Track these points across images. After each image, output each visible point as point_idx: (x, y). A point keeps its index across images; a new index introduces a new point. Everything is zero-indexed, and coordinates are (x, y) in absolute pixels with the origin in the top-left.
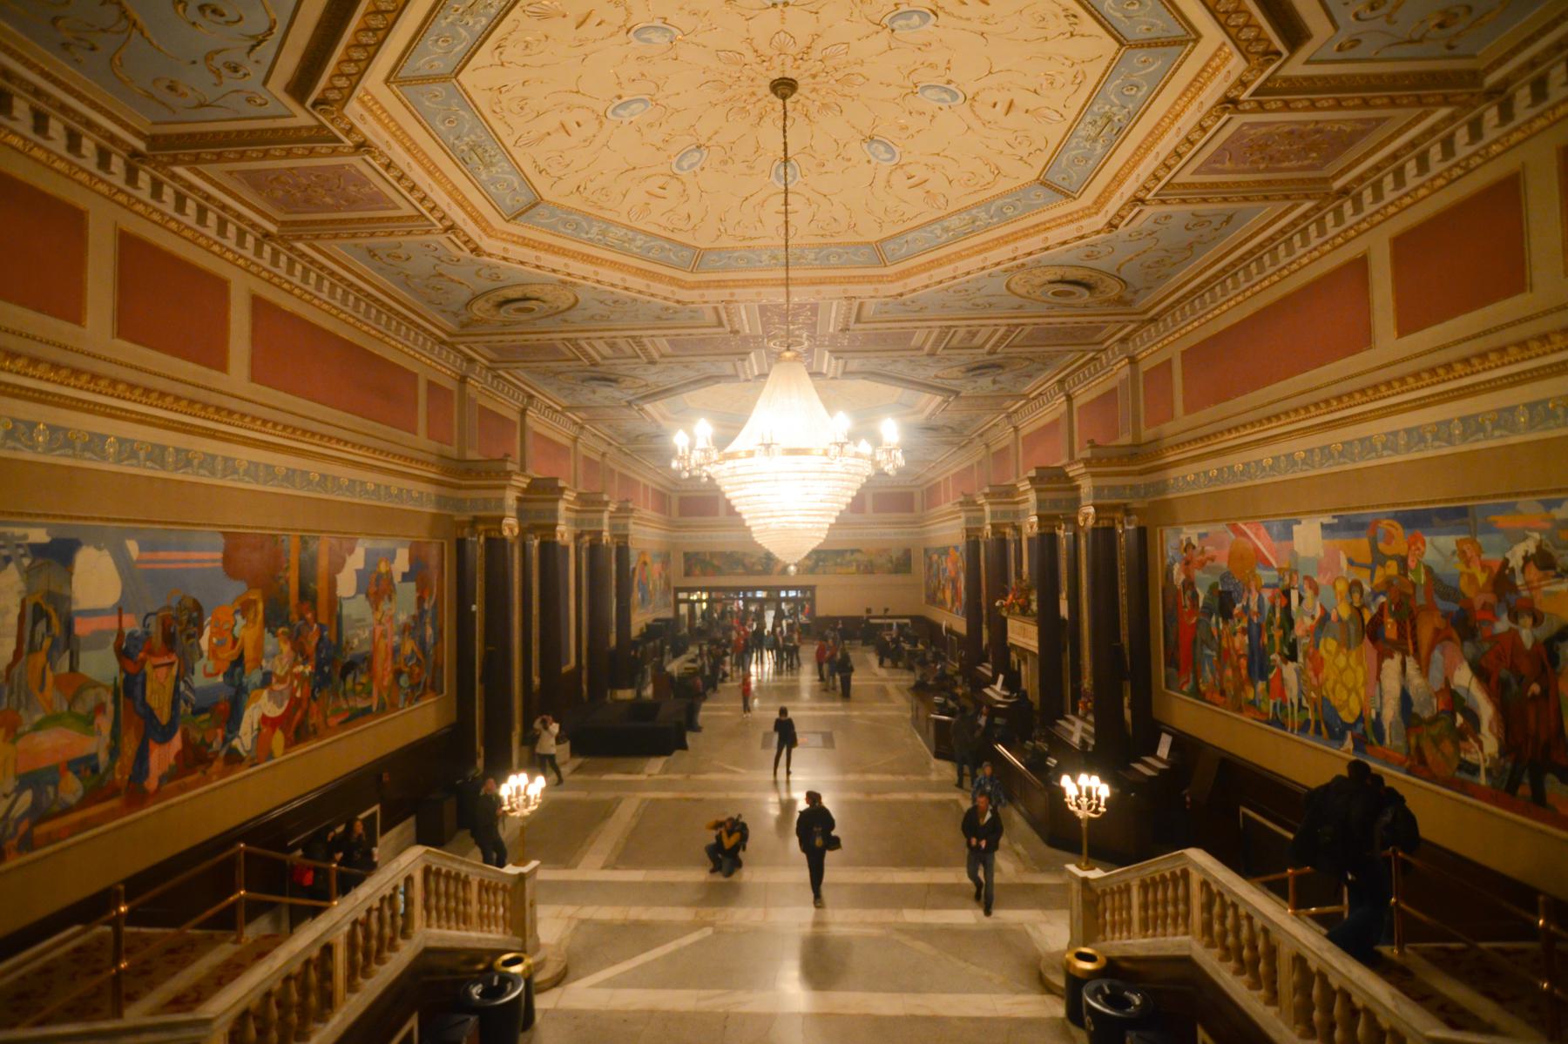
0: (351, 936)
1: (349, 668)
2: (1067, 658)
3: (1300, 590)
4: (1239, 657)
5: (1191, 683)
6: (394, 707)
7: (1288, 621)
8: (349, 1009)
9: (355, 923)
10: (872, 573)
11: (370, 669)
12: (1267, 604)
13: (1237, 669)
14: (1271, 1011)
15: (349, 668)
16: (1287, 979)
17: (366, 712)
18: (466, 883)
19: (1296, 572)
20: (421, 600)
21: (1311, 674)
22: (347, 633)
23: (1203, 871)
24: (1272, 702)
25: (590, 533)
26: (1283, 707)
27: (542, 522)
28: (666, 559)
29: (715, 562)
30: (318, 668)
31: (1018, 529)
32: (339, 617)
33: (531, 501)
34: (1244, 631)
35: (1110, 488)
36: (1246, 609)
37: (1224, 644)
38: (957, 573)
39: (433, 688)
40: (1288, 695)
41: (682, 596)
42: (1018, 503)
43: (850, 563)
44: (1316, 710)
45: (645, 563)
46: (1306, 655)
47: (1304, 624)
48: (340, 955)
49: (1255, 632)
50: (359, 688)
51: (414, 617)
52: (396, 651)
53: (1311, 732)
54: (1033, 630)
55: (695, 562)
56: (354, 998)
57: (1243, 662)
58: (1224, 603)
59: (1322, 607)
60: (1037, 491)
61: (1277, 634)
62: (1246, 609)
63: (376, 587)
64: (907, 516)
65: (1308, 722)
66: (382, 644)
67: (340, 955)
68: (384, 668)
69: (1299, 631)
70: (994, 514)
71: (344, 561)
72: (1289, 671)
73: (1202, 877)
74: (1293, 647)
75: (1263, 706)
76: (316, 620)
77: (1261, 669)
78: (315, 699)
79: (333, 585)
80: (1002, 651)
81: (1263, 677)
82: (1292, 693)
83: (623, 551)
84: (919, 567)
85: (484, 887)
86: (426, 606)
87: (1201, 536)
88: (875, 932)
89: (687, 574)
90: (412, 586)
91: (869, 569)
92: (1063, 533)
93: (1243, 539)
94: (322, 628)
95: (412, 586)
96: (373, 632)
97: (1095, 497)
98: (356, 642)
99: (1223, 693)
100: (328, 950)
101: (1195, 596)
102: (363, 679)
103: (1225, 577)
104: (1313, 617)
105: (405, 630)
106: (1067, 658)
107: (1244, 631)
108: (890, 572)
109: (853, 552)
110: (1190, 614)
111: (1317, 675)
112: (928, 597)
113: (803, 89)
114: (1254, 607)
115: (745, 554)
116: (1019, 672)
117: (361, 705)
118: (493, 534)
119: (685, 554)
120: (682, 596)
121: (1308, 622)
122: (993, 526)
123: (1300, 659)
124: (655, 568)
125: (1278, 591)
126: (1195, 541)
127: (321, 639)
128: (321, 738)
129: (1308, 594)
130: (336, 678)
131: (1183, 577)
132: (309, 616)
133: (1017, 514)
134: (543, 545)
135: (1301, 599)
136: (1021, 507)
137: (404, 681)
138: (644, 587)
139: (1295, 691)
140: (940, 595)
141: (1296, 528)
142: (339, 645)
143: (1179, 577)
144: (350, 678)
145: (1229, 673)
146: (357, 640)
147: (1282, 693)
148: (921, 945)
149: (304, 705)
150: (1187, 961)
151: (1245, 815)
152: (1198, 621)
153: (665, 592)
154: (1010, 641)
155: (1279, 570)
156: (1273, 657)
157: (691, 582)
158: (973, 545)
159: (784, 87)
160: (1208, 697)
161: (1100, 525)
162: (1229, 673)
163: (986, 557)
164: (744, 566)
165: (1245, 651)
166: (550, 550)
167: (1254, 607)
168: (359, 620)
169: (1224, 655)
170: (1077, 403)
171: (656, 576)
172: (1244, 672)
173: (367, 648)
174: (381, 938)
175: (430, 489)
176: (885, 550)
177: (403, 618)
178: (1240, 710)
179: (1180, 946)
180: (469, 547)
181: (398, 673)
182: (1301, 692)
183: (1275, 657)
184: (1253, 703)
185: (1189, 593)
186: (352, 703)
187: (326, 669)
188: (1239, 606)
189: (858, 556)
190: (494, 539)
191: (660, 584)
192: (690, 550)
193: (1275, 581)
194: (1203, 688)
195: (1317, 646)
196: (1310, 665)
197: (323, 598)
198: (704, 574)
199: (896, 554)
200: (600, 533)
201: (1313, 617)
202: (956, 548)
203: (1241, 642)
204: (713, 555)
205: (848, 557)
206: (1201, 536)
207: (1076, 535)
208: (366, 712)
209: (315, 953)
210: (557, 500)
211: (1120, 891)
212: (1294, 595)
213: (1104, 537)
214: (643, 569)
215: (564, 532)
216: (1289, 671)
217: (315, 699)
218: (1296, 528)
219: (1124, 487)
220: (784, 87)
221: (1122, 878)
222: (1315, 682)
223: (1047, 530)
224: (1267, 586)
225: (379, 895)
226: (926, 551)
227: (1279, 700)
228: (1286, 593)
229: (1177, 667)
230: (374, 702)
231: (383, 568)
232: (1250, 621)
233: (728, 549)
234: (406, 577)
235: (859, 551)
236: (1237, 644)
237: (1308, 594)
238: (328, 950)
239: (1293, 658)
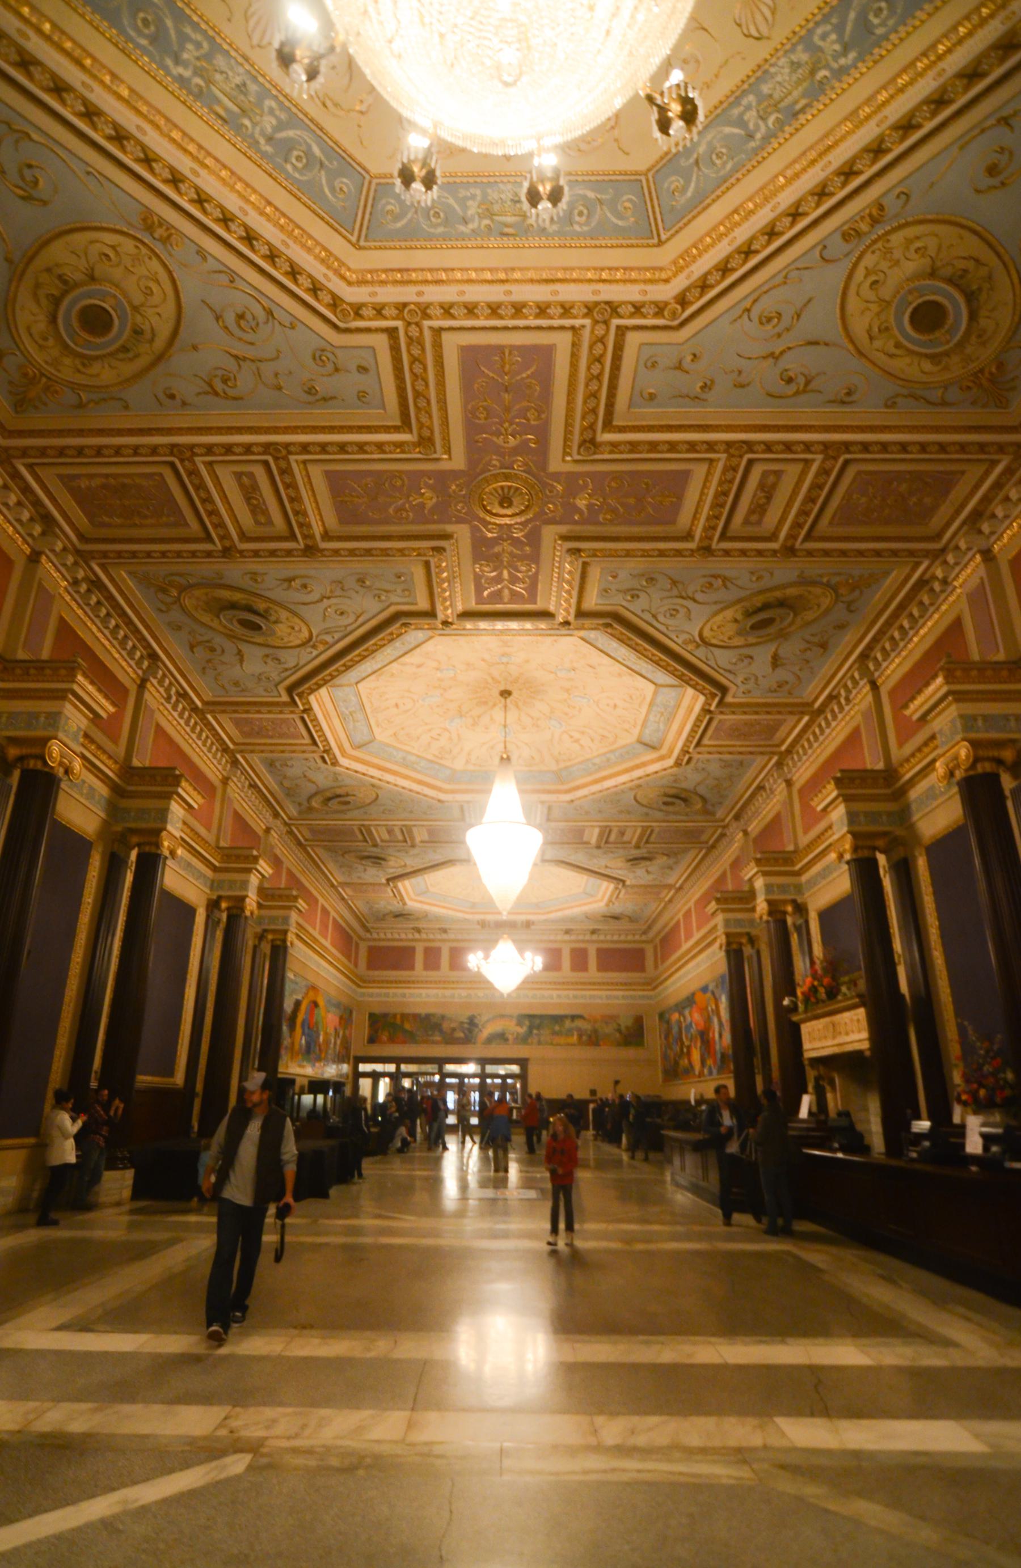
25: (229, 898)
27: (143, 825)
28: (346, 1017)
29: (407, 1026)
31: (801, 909)
33: (132, 795)
35: (986, 718)
42: (798, 874)
43: (569, 1033)
45: (315, 1004)
55: (387, 1028)
60: (848, 799)
64: (635, 976)
70: (769, 888)
84: (654, 1038)
88: (722, 1472)
89: (372, 1040)
91: (593, 1039)
97: (966, 728)
108: (619, 1045)
109: (573, 1018)
113: (515, 694)
115: (443, 1017)
118: (31, 764)
119: (371, 1015)
122: (770, 902)
133: (799, 888)
140: (684, 1062)
148: (871, 1512)
157: (375, 1050)
159: (506, 694)
161: (980, 769)
164: (441, 1031)
170: (884, 691)
171: (331, 1030)
176: (613, 1018)
189: (579, 1023)
190: (35, 773)
192: (377, 1010)
198: (392, 1040)
199: (626, 1022)
200: (243, 899)
204: (404, 1016)
205: (568, 1024)
210: (168, 796)
215: (183, 879)
219: (1006, 717)
220: (506, 694)
223: (866, 853)
226: (661, 1016)
233: (423, 1011)
235: (581, 1017)
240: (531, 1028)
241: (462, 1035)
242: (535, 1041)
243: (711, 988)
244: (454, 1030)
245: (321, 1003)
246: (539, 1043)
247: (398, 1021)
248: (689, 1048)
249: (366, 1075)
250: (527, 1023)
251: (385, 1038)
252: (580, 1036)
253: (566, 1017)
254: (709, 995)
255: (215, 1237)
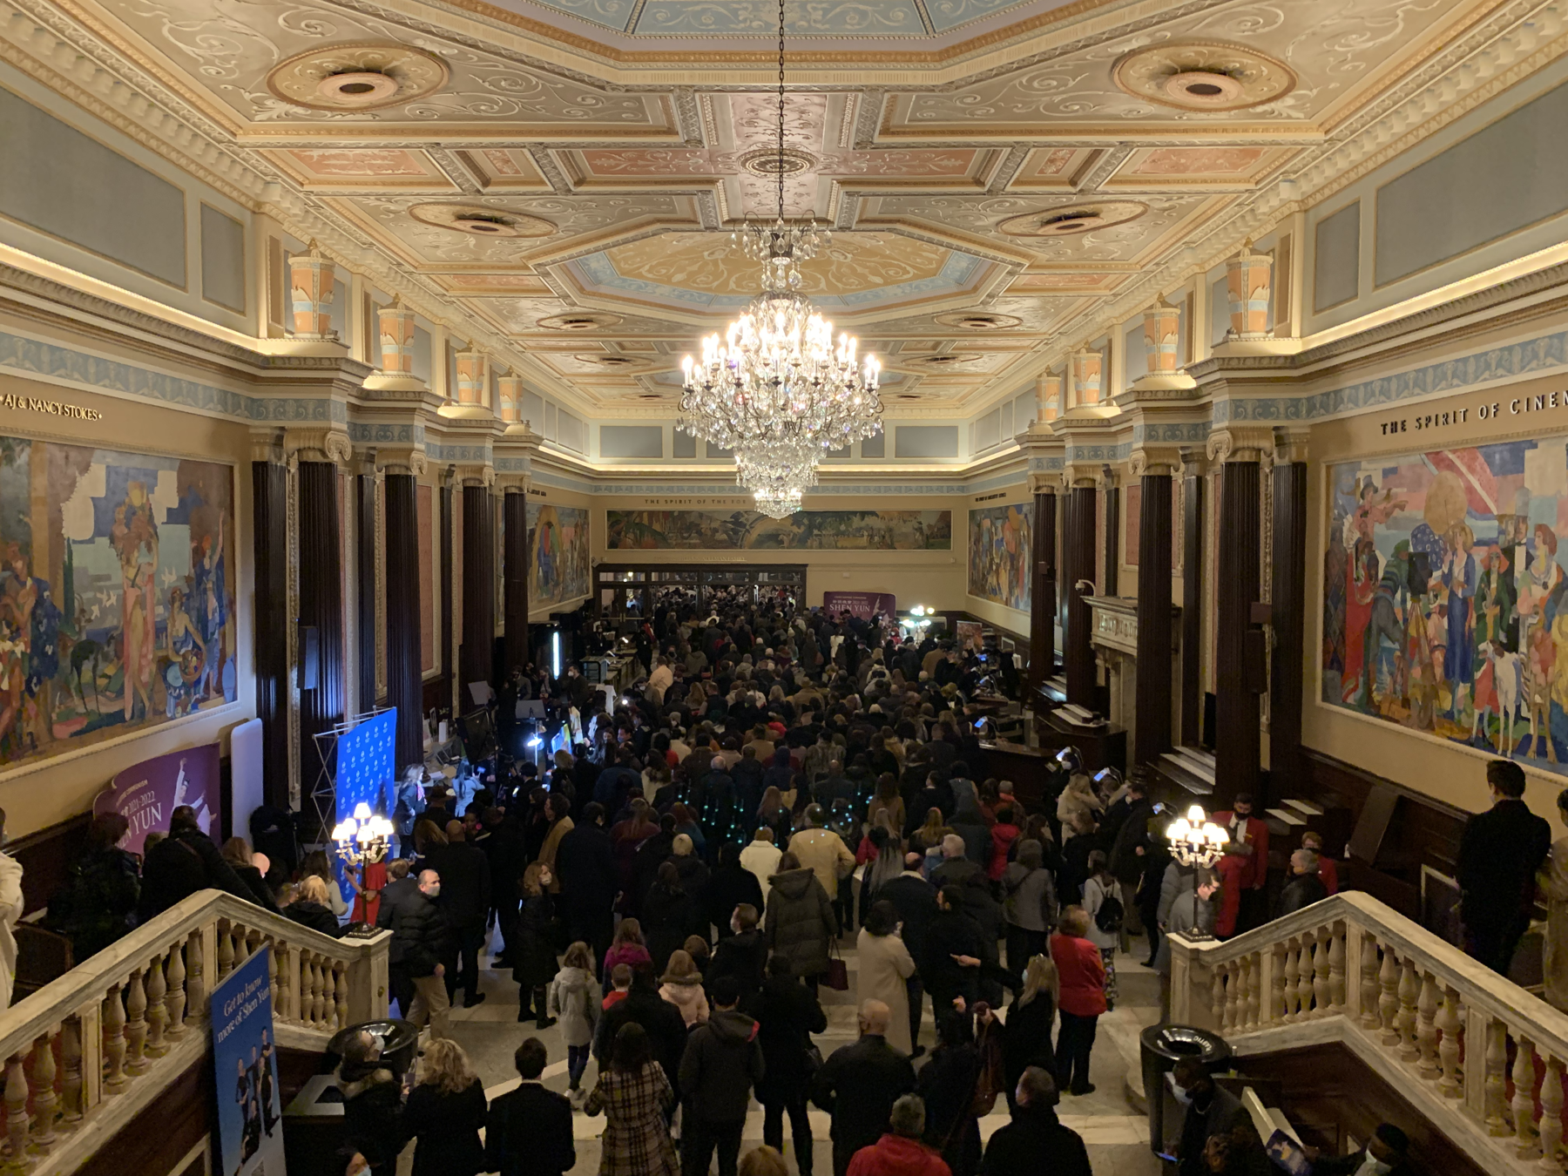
0: (107, 1005)
1: (86, 650)
2: (1178, 665)
3: (1530, 545)
4: (1433, 649)
5: (1360, 691)
6: (160, 715)
7: (1509, 593)
8: (110, 1113)
9: (113, 990)
10: (891, 547)
11: (119, 654)
12: (1479, 570)
13: (1428, 667)
14: (1453, 1104)
15: (86, 650)
16: (1482, 1051)
17: (116, 719)
18: (281, 951)
19: (1525, 519)
20: (198, 554)
21: (1537, 668)
22: (83, 596)
23: (1368, 919)
24: (1477, 713)
25: (463, 468)
26: (1493, 720)
29: (657, 527)
30: (36, 646)
32: (68, 571)
34: (1443, 611)
36: (1447, 578)
37: (1412, 632)
38: (1019, 545)
39: (220, 691)
40: (1501, 701)
41: (606, 577)
44: (1541, 721)
45: (549, 525)
46: (1531, 640)
47: (1531, 595)
48: (92, 1033)
49: (1455, 611)
50: (102, 682)
51: (188, 579)
52: (160, 630)
53: (1531, 753)
54: (1131, 623)
56: (114, 1102)
57: (1439, 656)
58: (1415, 570)
59: (1559, 568)
61: (1491, 612)
62: (1447, 578)
63: (125, 527)
65: (1528, 737)
66: (138, 617)
67: (92, 1033)
68: (140, 652)
69: (1522, 608)
71: (72, 485)
72: (1505, 666)
73: (1363, 929)
74: (1513, 632)
75: (1463, 717)
76: (30, 574)
77: (1464, 665)
78: (32, 694)
79: (56, 523)
80: (1084, 662)
81: (1467, 676)
82: (1507, 700)
83: (514, 502)
85: (307, 962)
86: (207, 563)
87: (1387, 473)
90: (183, 531)
92: (1182, 479)
93: (1448, 474)
94: (40, 585)
95: (183, 531)
96: (123, 600)
98: (96, 609)
99: (1406, 703)
100: (73, 1024)
101: (1374, 563)
102: (110, 670)
103: (1421, 532)
104: (1545, 586)
105: (172, 598)
106: (1178, 665)
107: (1443, 611)
109: (863, 514)
110: (1364, 590)
111: (1545, 671)
112: (973, 582)
114: (1459, 573)
116: (1107, 688)
117: (108, 708)
120: (606, 577)
121: (1538, 593)
122: (1076, 468)
123: (1523, 648)
124: (565, 533)
125: (1496, 549)
126: (1378, 481)
127: (40, 602)
128: (43, 755)
129: (1541, 551)
130: (65, 663)
131: (1357, 535)
132: (19, 565)
133: (1113, 452)
134: (391, 481)
135: (1530, 559)
136: (1122, 441)
137: (174, 676)
138: (547, 557)
139: (1512, 696)
140: (992, 580)
141: (1528, 454)
142: (70, 613)
143: (1350, 535)
144: (87, 666)
145: (1416, 672)
146: (99, 608)
147: (1493, 699)
149: (15, 704)
150: (1338, 1049)
151: (1429, 877)
152: (1375, 600)
153: (580, 572)
154: (1096, 640)
155: (1501, 518)
156: (1482, 647)
158: (1046, 502)
160: (1384, 711)
161: (1238, 459)
162: (1416, 672)
163: (1064, 535)
164: (699, 533)
165: (1443, 639)
166: (399, 487)
167: (1459, 573)
168: (99, 578)
169: (1410, 646)
172: (1439, 671)
173: (111, 622)
174: (152, 1020)
175: (212, 382)
176: (914, 514)
177: (170, 579)
178: (1430, 727)
179: (1327, 1030)
180: (274, 478)
181: (164, 664)
182: (1520, 695)
183: (1486, 646)
184: (1449, 715)
185: (1364, 558)
186: (92, 706)
187: (49, 649)
188: (1437, 574)
189: (869, 520)
191: (573, 560)
193: (1494, 535)
194: (1377, 697)
195: (1548, 628)
196: (1536, 656)
197: (40, 538)
198: (638, 544)
200: (480, 469)
201: (1545, 586)
202: (1019, 508)
203: (1437, 627)
206: (1387, 473)
207: (1200, 482)
208: (116, 719)
209: (54, 1028)
211: (1246, 965)
212: (1520, 554)
213: (1243, 476)
214: (545, 536)
216: (1505, 666)
217: (32, 694)
218: (1528, 454)
221: (1249, 944)
222: (1541, 679)
223: (1160, 471)
224: (1480, 543)
225: (151, 954)
227: (1487, 709)
228: (1509, 553)
229: (1341, 669)
230: (127, 704)
231: (136, 499)
232: (1452, 594)
234: (173, 516)
235: (873, 513)
236: (1431, 632)
237: (1541, 551)
238: (73, 1024)
239: (1512, 646)
240: (810, 528)
241: (725, 536)
242: (816, 544)
243: (1025, 509)
244: (715, 530)
245: (554, 521)
246: (821, 546)
247: (645, 521)
248: (998, 566)
249: (607, 585)
250: (806, 521)
251: (629, 541)
252: (871, 537)
253: (855, 513)
254: (1022, 517)
255: (745, 1137)
